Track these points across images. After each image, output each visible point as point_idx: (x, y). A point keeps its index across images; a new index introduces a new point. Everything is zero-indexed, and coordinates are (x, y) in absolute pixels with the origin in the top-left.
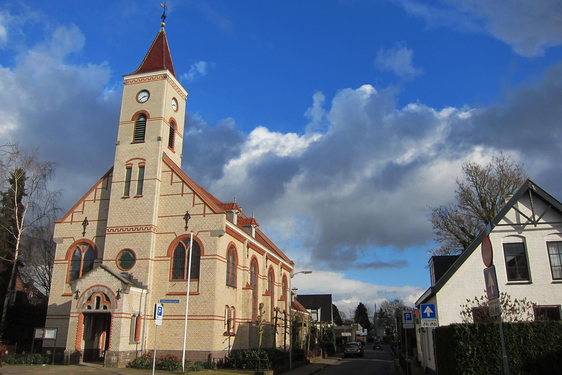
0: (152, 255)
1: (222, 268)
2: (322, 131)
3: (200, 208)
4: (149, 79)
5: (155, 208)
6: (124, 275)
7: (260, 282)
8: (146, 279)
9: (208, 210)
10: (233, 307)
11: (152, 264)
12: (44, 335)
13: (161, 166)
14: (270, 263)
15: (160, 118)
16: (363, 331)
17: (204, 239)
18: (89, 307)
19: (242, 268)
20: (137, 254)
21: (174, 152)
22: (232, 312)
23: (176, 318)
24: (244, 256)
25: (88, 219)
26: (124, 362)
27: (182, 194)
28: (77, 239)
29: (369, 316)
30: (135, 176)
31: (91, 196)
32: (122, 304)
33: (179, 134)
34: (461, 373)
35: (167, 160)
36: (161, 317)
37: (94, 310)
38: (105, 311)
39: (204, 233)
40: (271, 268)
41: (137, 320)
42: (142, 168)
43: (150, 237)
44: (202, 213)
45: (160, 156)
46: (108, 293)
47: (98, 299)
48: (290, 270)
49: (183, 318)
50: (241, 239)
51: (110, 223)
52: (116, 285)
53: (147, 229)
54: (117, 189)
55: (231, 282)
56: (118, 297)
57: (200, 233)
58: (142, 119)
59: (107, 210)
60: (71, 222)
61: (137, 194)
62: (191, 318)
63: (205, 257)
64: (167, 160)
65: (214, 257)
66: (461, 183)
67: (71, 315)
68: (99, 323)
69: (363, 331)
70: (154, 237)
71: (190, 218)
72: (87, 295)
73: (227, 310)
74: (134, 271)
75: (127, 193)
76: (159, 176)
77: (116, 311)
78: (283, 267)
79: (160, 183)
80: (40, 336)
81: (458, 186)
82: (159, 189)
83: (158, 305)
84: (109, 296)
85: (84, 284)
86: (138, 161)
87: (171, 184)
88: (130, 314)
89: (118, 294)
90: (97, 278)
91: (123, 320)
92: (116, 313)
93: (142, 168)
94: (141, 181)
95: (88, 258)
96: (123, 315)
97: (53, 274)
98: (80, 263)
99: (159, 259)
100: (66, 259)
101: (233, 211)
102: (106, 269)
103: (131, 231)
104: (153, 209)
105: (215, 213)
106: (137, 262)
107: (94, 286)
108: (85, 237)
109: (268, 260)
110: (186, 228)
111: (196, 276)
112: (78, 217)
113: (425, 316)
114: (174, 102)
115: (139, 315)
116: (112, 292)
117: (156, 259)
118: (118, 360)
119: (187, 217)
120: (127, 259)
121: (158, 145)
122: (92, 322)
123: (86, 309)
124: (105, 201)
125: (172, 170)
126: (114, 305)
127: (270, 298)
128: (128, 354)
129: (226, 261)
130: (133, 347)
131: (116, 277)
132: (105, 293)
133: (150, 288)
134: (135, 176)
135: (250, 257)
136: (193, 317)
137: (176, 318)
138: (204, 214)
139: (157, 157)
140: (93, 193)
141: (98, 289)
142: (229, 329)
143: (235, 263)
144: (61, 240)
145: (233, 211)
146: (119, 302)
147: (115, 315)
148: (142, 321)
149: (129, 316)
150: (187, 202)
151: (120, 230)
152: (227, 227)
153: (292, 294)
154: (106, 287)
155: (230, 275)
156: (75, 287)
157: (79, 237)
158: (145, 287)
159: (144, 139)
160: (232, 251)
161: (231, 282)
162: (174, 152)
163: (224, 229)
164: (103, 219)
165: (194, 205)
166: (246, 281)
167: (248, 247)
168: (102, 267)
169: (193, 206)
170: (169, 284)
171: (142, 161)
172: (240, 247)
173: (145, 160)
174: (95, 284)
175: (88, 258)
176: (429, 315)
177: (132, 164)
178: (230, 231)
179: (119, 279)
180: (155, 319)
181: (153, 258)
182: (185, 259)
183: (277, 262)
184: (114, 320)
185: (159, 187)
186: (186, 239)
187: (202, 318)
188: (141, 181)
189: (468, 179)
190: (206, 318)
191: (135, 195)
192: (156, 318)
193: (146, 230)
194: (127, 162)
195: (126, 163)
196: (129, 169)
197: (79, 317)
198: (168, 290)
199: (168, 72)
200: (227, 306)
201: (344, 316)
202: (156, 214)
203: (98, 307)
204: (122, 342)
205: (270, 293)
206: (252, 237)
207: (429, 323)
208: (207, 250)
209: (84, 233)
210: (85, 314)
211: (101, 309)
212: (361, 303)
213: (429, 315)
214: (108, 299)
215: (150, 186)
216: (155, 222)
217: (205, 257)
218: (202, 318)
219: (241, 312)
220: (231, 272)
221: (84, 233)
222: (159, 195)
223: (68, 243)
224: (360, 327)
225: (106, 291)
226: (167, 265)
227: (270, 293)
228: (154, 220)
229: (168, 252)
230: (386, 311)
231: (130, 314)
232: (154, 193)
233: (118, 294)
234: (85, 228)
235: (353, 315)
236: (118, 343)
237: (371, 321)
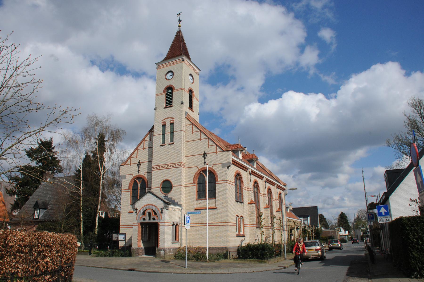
0: (183, 183)
1: (231, 189)
3: (213, 148)
5: (182, 150)
6: (166, 198)
7: (261, 199)
8: (180, 199)
9: (219, 150)
10: (242, 217)
11: (183, 189)
12: (118, 238)
13: (185, 122)
14: (268, 185)
15: (182, 89)
16: (345, 233)
17: (218, 170)
18: (144, 219)
19: (247, 189)
21: (193, 111)
22: (242, 220)
23: (202, 225)
24: (248, 181)
25: (140, 162)
26: (170, 256)
27: (200, 139)
28: (134, 175)
29: (349, 221)
31: (141, 146)
32: (165, 216)
33: (197, 100)
35: (188, 118)
36: (189, 224)
37: (147, 220)
38: (154, 221)
39: (217, 165)
40: (269, 189)
41: (176, 226)
42: (172, 124)
43: (181, 171)
45: (184, 115)
46: (155, 209)
47: (149, 213)
48: (283, 190)
49: (210, 224)
50: (245, 169)
51: (154, 163)
52: (160, 204)
53: (178, 165)
54: (157, 139)
55: (239, 199)
56: (162, 212)
58: (170, 91)
59: (152, 154)
60: (130, 164)
61: (170, 142)
62: (205, 225)
63: (219, 182)
64: (188, 118)
65: (225, 182)
66: (408, 115)
68: (150, 231)
69: (345, 233)
70: (183, 171)
71: (207, 156)
72: (142, 211)
73: (237, 219)
74: (172, 195)
75: (164, 141)
76: (184, 128)
77: (161, 221)
78: (279, 187)
79: (185, 133)
80: (116, 239)
81: (406, 118)
82: (185, 137)
83: (187, 216)
84: (156, 211)
85: (140, 204)
90: (147, 200)
91: (166, 227)
93: (172, 124)
94: (172, 133)
95: (140, 187)
96: (166, 224)
97: (122, 198)
98: (138, 191)
99: (188, 185)
100: (129, 189)
101: (238, 149)
102: (153, 194)
104: (181, 152)
106: (173, 188)
107: (146, 205)
108: (140, 174)
109: (251, 175)
110: (205, 163)
111: (213, 195)
112: (135, 161)
113: (380, 214)
114: (190, 77)
116: (158, 209)
117: (186, 185)
118: (165, 254)
119: (205, 155)
120: (167, 186)
121: (182, 108)
122: (147, 229)
123: (142, 221)
124: (151, 148)
125: (193, 124)
126: (159, 217)
127: (269, 209)
128: (172, 250)
129: (234, 184)
130: (176, 246)
131: (160, 198)
132: (154, 209)
133: (183, 205)
135: (267, 188)
136: (212, 225)
137: (202, 225)
138: (216, 152)
139: (182, 115)
140: (143, 143)
141: (149, 207)
142: (239, 231)
143: (242, 186)
144: (124, 177)
145: (238, 149)
146: (163, 215)
147: (160, 224)
148: (180, 227)
150: (204, 145)
151: (161, 167)
153: (287, 208)
154: (154, 206)
155: (239, 194)
156: (134, 206)
157: (136, 174)
158: (180, 205)
159: (172, 104)
160: (238, 176)
161: (239, 199)
162: (193, 111)
163: (231, 162)
164: (150, 161)
165: (209, 146)
166: (250, 198)
167: (250, 174)
168: (150, 193)
170: (196, 202)
171: (172, 119)
172: (244, 175)
173: (174, 118)
174: (147, 204)
175: (140, 187)
176: (383, 214)
179: (161, 200)
181: (184, 185)
182: (206, 184)
183: (273, 184)
184: (161, 228)
185: (185, 136)
186: (205, 171)
188: (172, 133)
189: (414, 112)
190: (222, 224)
191: (169, 143)
193: (178, 166)
196: (164, 126)
197: (138, 226)
198: (196, 207)
199: (184, 57)
200: (237, 216)
201: (331, 223)
202: (183, 155)
203: (150, 219)
204: (166, 241)
205: (270, 206)
206: (254, 168)
207: (384, 219)
208: (220, 177)
209: (139, 171)
210: (142, 224)
211: (152, 221)
212: (342, 213)
213: (383, 214)
214: (155, 213)
216: (184, 160)
217: (219, 182)
219: (248, 220)
220: (239, 192)
221: (139, 171)
222: (185, 141)
223: (129, 179)
224: (342, 230)
225: (154, 208)
226: (194, 189)
227: (270, 206)
228: (182, 159)
229: (194, 180)
230: (362, 218)
232: (181, 141)
234: (139, 168)
235: (337, 221)
236: (164, 242)
237: (351, 225)
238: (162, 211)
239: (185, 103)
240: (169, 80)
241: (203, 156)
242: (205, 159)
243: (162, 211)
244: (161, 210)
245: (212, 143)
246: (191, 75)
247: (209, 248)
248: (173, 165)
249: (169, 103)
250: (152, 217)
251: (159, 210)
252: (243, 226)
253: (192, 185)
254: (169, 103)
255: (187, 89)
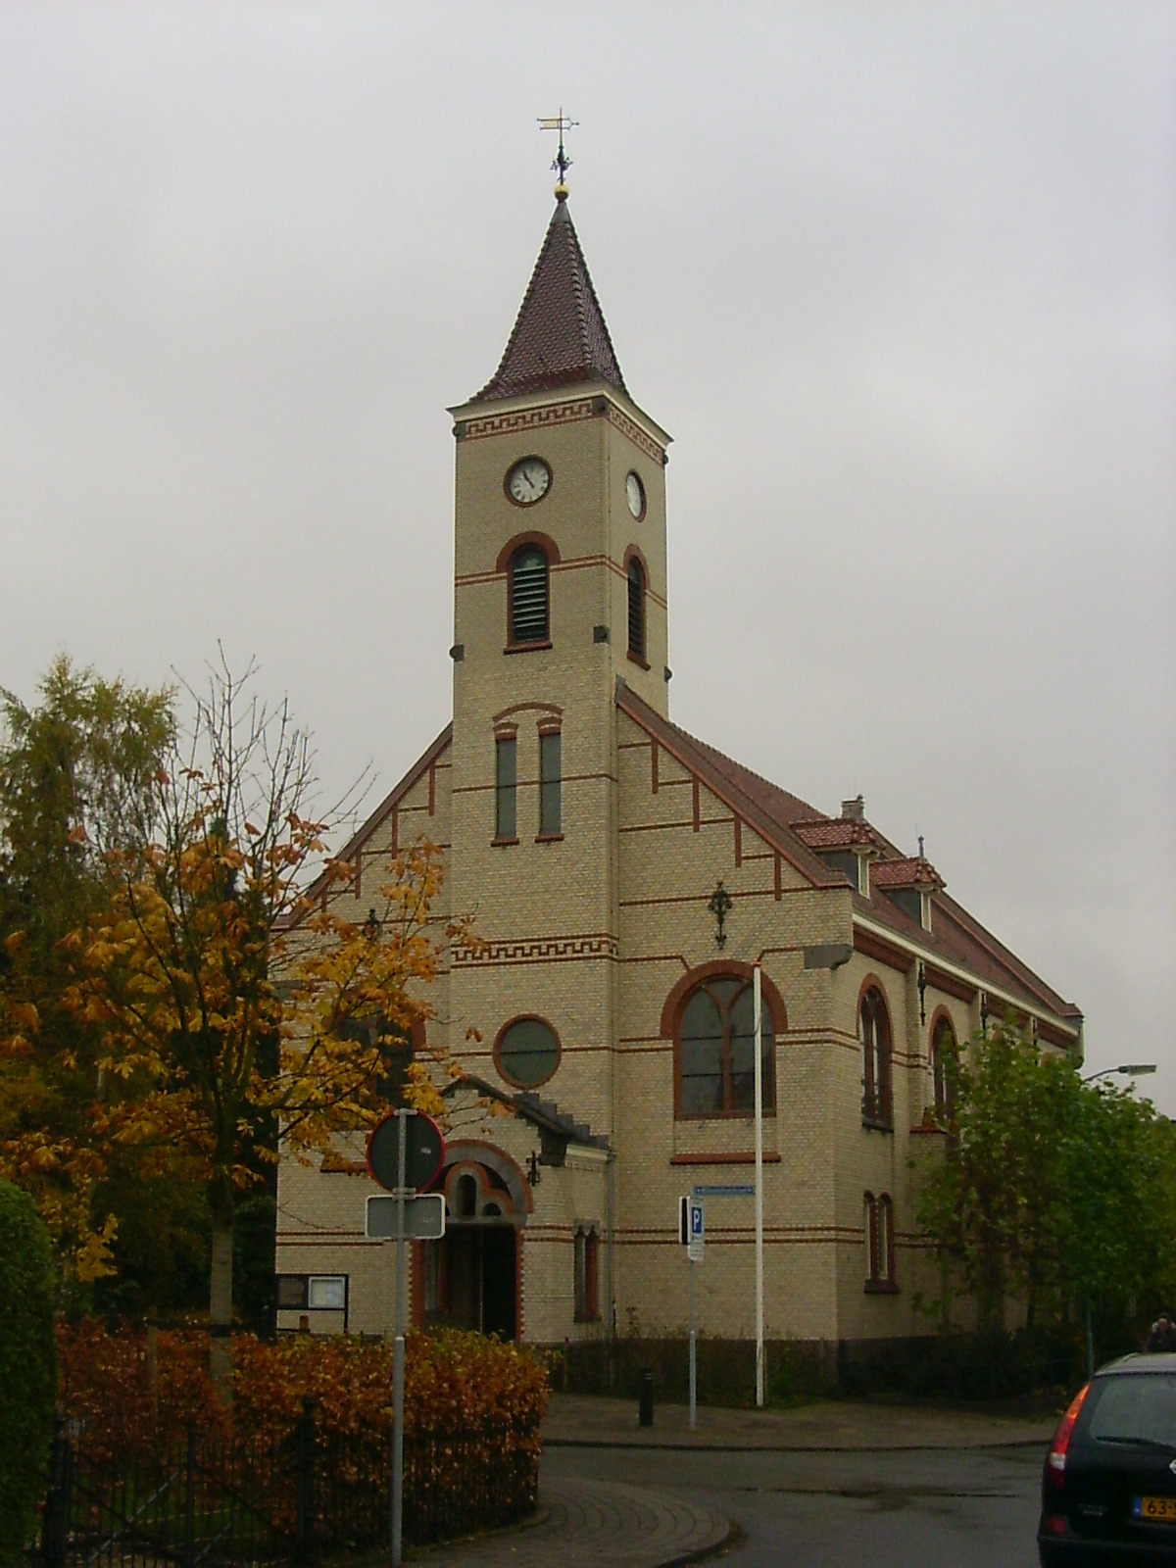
2: (1095, 1119)
4: (552, 417)
9: (790, 879)
20: (562, 1033)
21: (647, 668)
27: (696, 824)
30: (527, 764)
34: (4, 974)
39: (784, 956)
42: (549, 736)
44: (771, 887)
56: (533, 1178)
57: (768, 957)
58: (531, 565)
62: (744, 1236)
63: (791, 1038)
67: (278, 1239)
71: (729, 906)
86: (536, 715)
87: (655, 791)
88: (569, 1229)
89: (534, 1167)
92: (533, 1228)
93: (549, 736)
96: (832, 1234)
103: (535, 956)
105: (815, 887)
110: (721, 939)
115: (592, 1232)
116: (512, 1162)
119: (720, 902)
134: (527, 764)
138: (778, 893)
147: (526, 1234)
148: (601, 1248)
149: (565, 1235)
152: (859, 932)
160: (873, 1006)
162: (647, 668)
169: (738, 865)
171: (547, 714)
173: (560, 712)
177: (516, 726)
178: (867, 944)
180: (685, 1242)
187: (793, 1236)
192: (689, 1239)
194: (496, 719)
195: (493, 724)
196: (505, 741)
200: (869, 1196)
211: (480, 1219)
215: (587, 801)
217: (791, 1038)
218: (793, 1236)
231: (569, 1229)
233: (534, 1167)
238: (534, 1173)
239: (613, 636)
240: (531, 503)
241: (711, 907)
242: (721, 921)
243: (534, 1173)
244: (526, 1169)
245: (757, 842)
246: (634, 474)
247: (702, 1343)
248: (561, 944)
249: (529, 631)
250: (481, 1204)
251: (518, 1169)
252: (890, 1239)
253: (657, 1045)
254: (529, 631)
255: (619, 558)
